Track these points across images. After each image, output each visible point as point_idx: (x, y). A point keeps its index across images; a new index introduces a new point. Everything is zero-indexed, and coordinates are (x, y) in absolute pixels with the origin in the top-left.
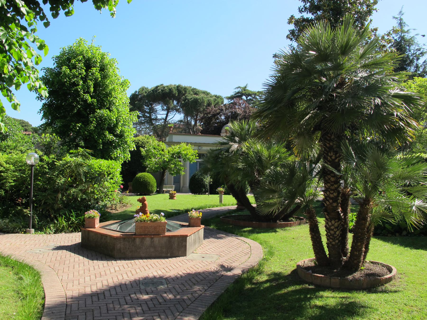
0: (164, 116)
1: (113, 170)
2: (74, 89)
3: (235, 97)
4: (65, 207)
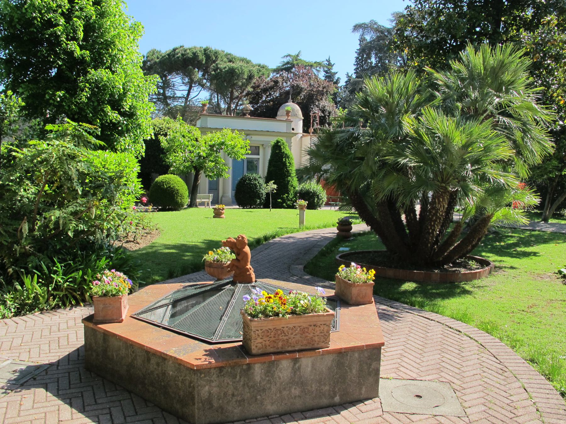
0: (185, 93)
2: (49, 32)
3: (282, 70)
4: (40, 250)
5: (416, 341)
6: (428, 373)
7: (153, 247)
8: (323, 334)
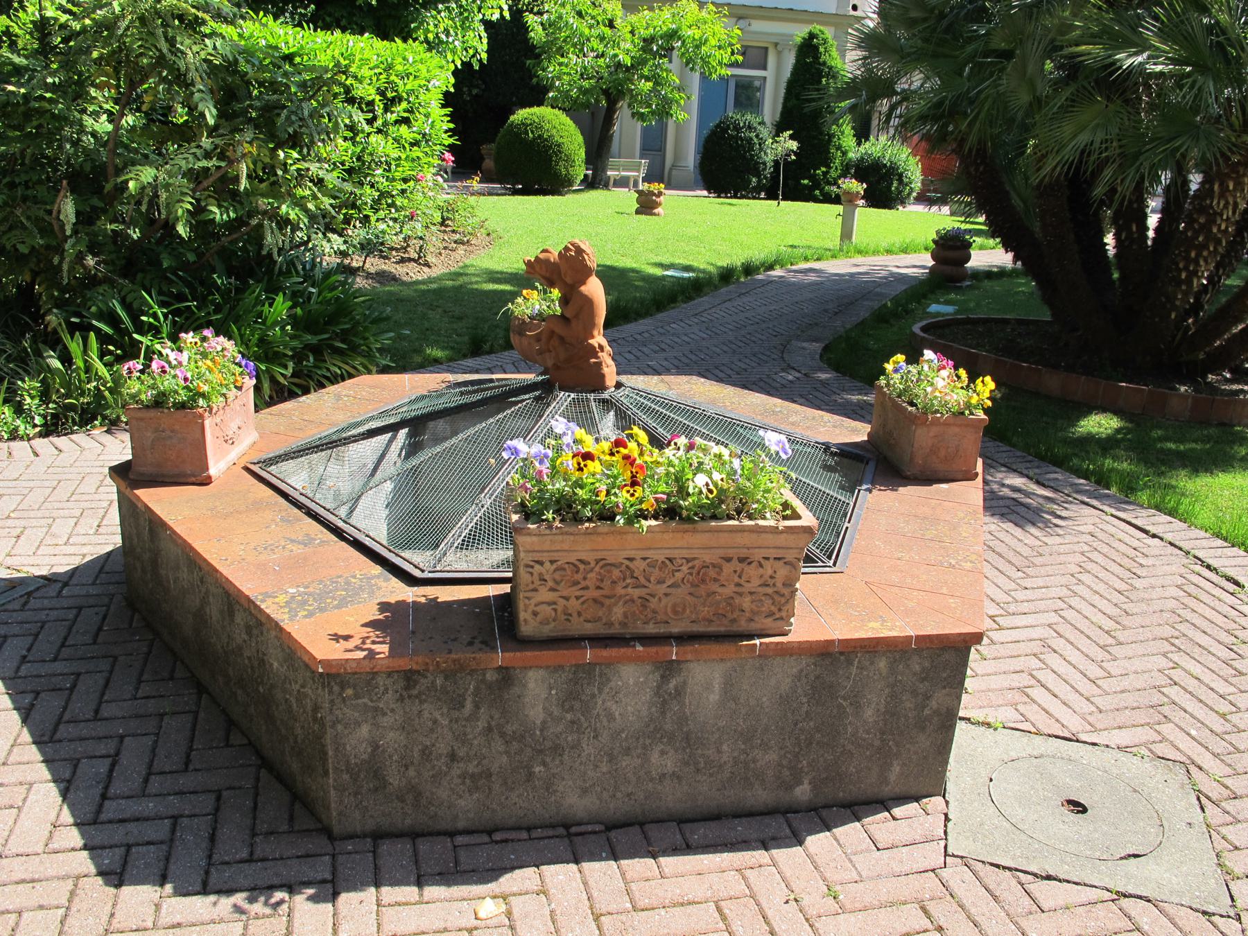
1: (411, 84)
5: (1096, 600)
6: (1121, 718)
7: (461, 274)
8: (769, 590)
